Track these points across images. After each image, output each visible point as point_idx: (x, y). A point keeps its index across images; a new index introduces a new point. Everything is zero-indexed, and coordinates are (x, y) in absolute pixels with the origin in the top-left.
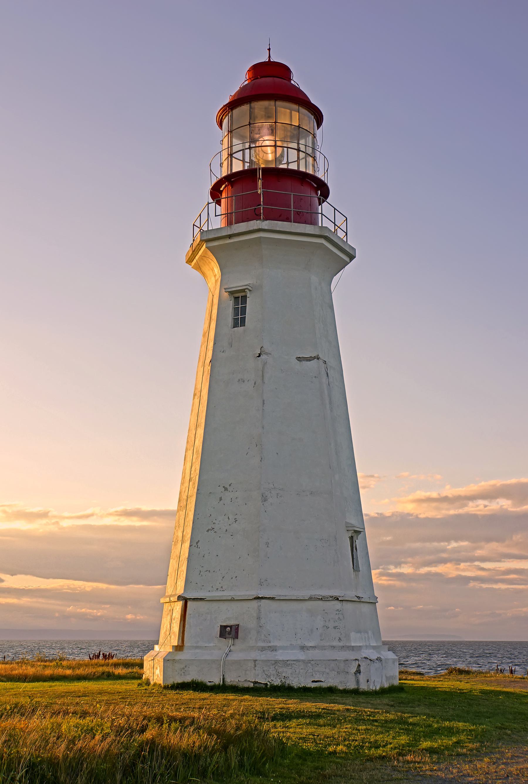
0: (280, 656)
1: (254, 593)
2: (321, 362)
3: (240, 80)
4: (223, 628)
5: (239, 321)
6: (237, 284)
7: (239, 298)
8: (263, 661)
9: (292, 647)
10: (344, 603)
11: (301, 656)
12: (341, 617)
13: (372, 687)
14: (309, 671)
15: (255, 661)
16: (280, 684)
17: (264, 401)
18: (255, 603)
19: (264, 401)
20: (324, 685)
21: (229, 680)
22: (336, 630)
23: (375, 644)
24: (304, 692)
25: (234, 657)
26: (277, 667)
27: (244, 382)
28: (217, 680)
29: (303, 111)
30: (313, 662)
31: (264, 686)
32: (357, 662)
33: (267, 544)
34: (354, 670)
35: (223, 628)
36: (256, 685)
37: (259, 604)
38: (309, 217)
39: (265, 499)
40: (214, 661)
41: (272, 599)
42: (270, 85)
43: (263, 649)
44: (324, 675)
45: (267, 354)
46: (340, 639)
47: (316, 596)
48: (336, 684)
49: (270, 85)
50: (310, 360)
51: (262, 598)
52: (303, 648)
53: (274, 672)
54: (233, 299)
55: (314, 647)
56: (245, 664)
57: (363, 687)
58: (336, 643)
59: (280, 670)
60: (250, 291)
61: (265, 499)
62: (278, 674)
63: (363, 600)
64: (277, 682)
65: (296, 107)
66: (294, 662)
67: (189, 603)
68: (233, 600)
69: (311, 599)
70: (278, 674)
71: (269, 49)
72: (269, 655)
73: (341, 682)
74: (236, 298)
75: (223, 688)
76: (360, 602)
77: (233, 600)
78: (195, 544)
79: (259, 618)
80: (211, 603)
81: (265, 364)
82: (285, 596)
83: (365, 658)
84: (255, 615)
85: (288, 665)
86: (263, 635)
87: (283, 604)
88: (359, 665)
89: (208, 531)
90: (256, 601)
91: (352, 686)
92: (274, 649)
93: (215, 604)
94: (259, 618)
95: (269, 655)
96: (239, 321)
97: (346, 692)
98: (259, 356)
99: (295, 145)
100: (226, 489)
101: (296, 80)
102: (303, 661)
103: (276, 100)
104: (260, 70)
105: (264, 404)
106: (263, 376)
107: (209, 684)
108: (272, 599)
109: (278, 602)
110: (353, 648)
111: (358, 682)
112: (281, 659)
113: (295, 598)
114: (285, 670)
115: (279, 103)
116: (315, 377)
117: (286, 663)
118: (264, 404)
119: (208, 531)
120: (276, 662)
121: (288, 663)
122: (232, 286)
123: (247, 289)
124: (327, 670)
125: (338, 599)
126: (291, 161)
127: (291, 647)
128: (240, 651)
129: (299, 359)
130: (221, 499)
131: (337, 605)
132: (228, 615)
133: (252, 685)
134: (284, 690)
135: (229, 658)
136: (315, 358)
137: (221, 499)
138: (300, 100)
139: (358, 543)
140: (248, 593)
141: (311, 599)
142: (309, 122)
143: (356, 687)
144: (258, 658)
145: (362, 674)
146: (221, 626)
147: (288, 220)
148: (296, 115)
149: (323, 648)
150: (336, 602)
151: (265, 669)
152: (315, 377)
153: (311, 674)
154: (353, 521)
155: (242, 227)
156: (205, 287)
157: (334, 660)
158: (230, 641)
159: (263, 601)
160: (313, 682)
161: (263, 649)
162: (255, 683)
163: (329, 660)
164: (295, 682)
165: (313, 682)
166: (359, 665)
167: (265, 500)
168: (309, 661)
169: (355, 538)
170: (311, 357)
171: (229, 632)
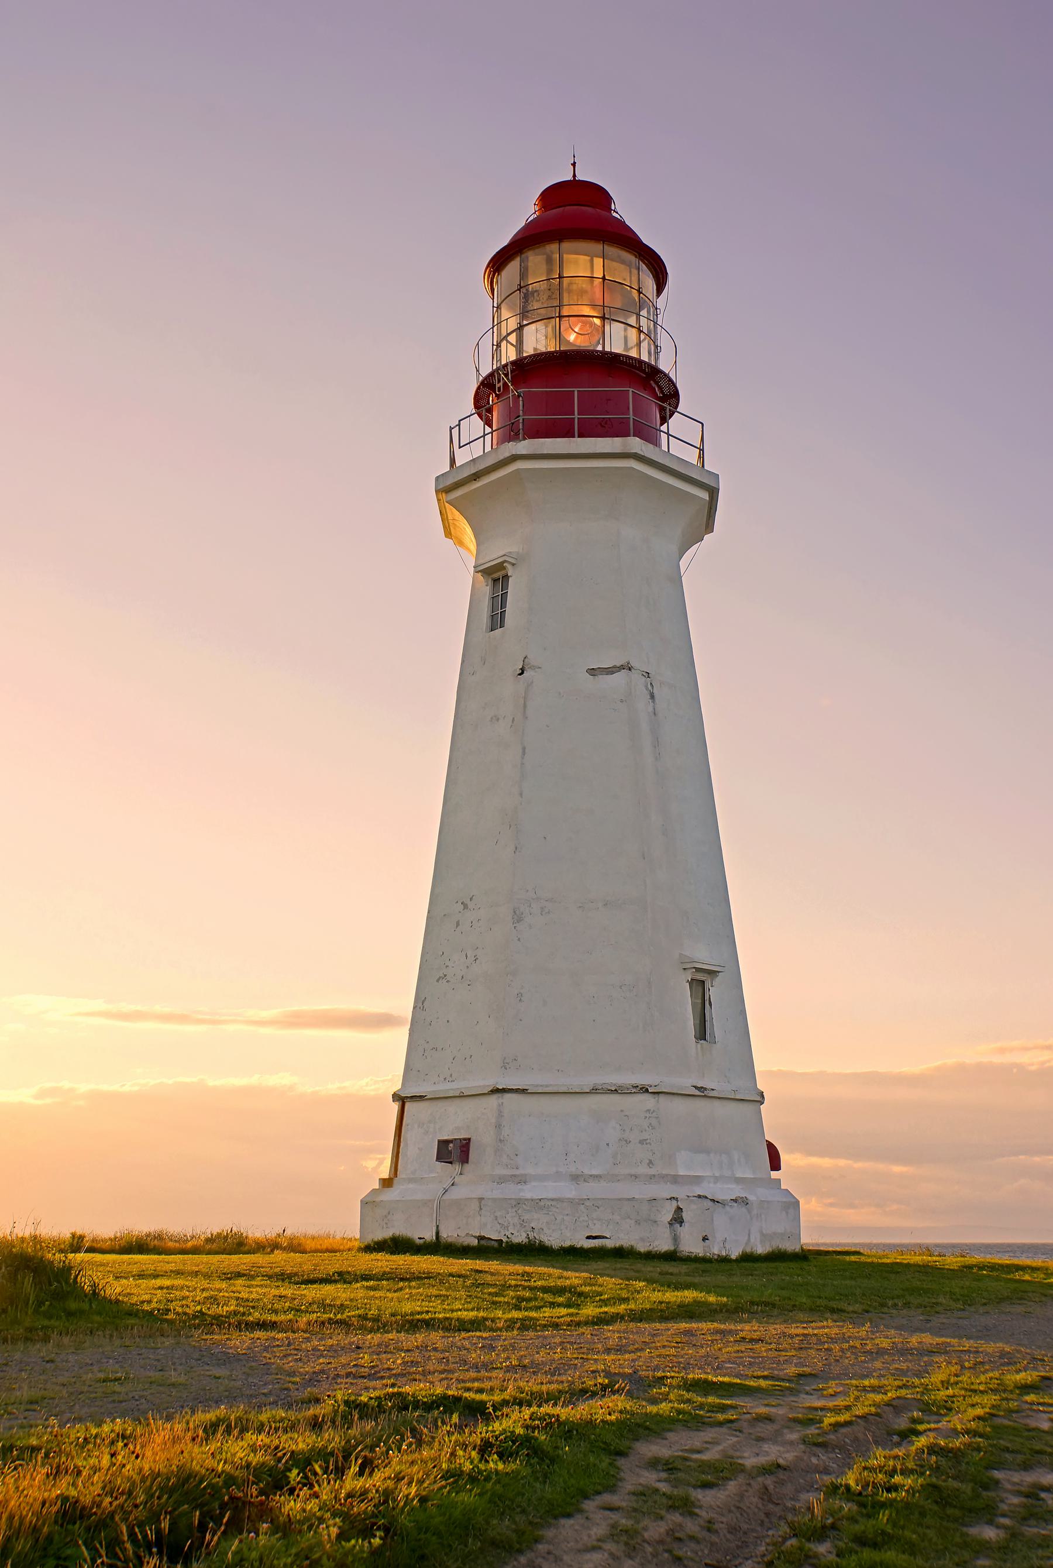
0: (529, 1192)
1: (491, 1082)
2: (635, 676)
3: (525, 211)
4: (443, 1144)
5: (497, 620)
6: (494, 555)
7: (496, 576)
8: (494, 1200)
9: (558, 1176)
10: (662, 1097)
11: (570, 1191)
12: (654, 1122)
13: (716, 1250)
14: (581, 1219)
15: (481, 1199)
16: (526, 1241)
17: (524, 749)
18: (494, 1100)
19: (524, 749)
20: (609, 1244)
21: (449, 1234)
22: (645, 1146)
23: (749, 1175)
24: (572, 1255)
25: (455, 1194)
26: (520, 1211)
27: (498, 720)
28: (429, 1236)
29: (612, 250)
30: (587, 1203)
31: (496, 1244)
32: (674, 1204)
33: (520, 995)
34: (669, 1217)
35: (443, 1144)
36: (483, 1242)
37: (500, 1101)
38: (650, 436)
39: (518, 918)
40: (426, 1203)
41: (523, 1091)
42: (576, 213)
43: (502, 1180)
44: (611, 1227)
45: (533, 668)
46: (650, 1162)
47: (604, 1086)
48: (633, 1243)
49: (576, 213)
50: (612, 673)
51: (504, 1091)
52: (575, 1178)
53: (516, 1220)
54: (490, 582)
55: (597, 1177)
56: (475, 1205)
57: (691, 1245)
58: (643, 1170)
59: (526, 1217)
60: (513, 565)
61: (518, 918)
62: (523, 1223)
63: (712, 1094)
64: (519, 1238)
65: (598, 247)
66: (553, 1203)
67: (407, 1105)
68: (462, 1096)
69: (595, 1091)
70: (523, 1223)
71: (574, 165)
72: (511, 1191)
73: (642, 1240)
74: (495, 581)
75: (437, 1247)
76: (705, 1096)
77: (462, 1096)
78: (420, 1005)
79: (498, 1126)
80: (435, 1103)
81: (530, 685)
82: (547, 1086)
83: (699, 1196)
84: (493, 1120)
85: (541, 1208)
86: (505, 1156)
87: (544, 1101)
88: (679, 1209)
89: (438, 981)
90: (494, 1097)
91: (664, 1245)
92: (522, 1180)
93: (441, 1104)
94: (498, 1126)
95: (511, 1191)
96: (497, 620)
97: (650, 1256)
98: (522, 673)
99: (632, 320)
100: (465, 906)
101: (624, 209)
102: (571, 1201)
103: (560, 241)
104: (552, 196)
105: (524, 753)
106: (525, 706)
107: (418, 1242)
108: (523, 1091)
109: (535, 1097)
110: (675, 1179)
111: (676, 1239)
112: (528, 1196)
113: (555, 1089)
114: (536, 1216)
115: (566, 245)
116: (622, 701)
117: (538, 1204)
118: (524, 753)
119: (438, 981)
120: (519, 1202)
121: (542, 1203)
122: (488, 559)
123: (505, 561)
124: (617, 1218)
125: (647, 1091)
126: (617, 340)
127: (561, 1179)
128: (469, 1184)
129: (592, 672)
130: (458, 924)
131: (649, 1101)
132: (454, 1122)
133: (475, 1242)
134: (533, 1251)
135: (444, 1197)
136: (622, 668)
137: (458, 924)
138: (623, 239)
139: (714, 992)
140: (482, 1083)
141: (595, 1091)
142: (649, 284)
143: (672, 1248)
144: (488, 1195)
145: (686, 1225)
146: (439, 1141)
147: (569, 434)
148: (598, 262)
149: (614, 1178)
150: (646, 1096)
151: (498, 1214)
152: (622, 701)
153: (585, 1224)
154: (704, 955)
155: (524, 446)
156: (449, 570)
157: (629, 1199)
158: (457, 1167)
159: (508, 1096)
160: (588, 1238)
161: (502, 1180)
162: (481, 1238)
163: (619, 1200)
164: (554, 1239)
165: (588, 1238)
166: (679, 1209)
167: (520, 920)
168: (582, 1201)
169: (707, 985)
170: (614, 667)
171: (455, 1152)
